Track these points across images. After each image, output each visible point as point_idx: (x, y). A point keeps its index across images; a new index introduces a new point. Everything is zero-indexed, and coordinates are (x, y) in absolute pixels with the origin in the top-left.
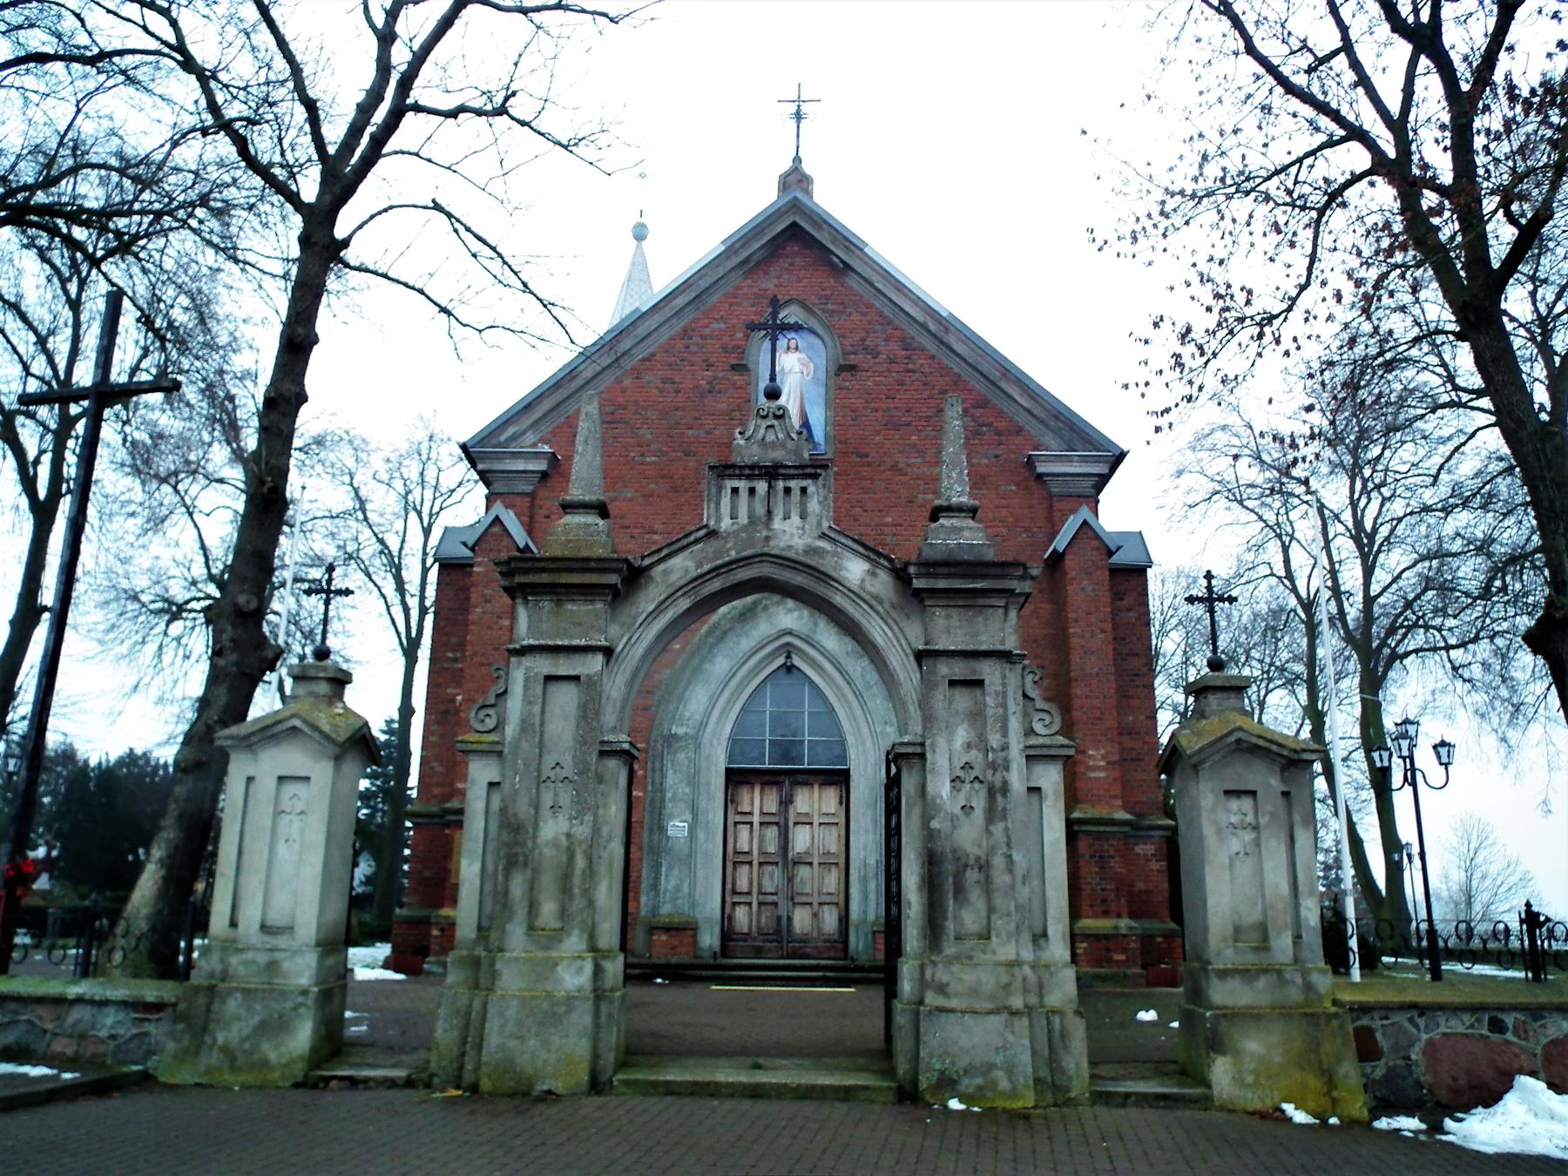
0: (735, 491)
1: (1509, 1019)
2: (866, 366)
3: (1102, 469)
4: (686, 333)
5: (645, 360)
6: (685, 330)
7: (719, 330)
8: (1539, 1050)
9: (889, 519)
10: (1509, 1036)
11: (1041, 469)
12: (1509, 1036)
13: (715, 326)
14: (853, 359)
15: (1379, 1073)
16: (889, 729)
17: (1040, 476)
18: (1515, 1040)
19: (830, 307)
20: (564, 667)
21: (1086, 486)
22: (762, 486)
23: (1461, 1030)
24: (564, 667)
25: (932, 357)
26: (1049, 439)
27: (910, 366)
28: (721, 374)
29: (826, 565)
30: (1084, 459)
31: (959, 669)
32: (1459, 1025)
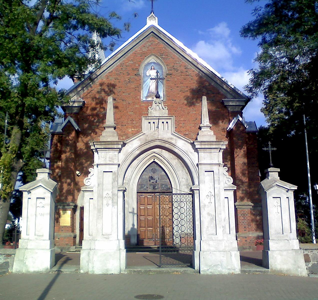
2: (174, 74)
3: (243, 104)
4: (121, 65)
5: (109, 73)
6: (121, 64)
9: (182, 119)
11: (226, 104)
13: (130, 62)
14: (171, 72)
15: (310, 265)
16: (183, 180)
19: (163, 56)
20: (107, 168)
21: (237, 109)
22: (156, 121)
24: (107, 168)
25: (194, 71)
26: (229, 96)
27: (187, 74)
28: (132, 77)
29: (173, 142)
30: (238, 101)
31: (209, 168)
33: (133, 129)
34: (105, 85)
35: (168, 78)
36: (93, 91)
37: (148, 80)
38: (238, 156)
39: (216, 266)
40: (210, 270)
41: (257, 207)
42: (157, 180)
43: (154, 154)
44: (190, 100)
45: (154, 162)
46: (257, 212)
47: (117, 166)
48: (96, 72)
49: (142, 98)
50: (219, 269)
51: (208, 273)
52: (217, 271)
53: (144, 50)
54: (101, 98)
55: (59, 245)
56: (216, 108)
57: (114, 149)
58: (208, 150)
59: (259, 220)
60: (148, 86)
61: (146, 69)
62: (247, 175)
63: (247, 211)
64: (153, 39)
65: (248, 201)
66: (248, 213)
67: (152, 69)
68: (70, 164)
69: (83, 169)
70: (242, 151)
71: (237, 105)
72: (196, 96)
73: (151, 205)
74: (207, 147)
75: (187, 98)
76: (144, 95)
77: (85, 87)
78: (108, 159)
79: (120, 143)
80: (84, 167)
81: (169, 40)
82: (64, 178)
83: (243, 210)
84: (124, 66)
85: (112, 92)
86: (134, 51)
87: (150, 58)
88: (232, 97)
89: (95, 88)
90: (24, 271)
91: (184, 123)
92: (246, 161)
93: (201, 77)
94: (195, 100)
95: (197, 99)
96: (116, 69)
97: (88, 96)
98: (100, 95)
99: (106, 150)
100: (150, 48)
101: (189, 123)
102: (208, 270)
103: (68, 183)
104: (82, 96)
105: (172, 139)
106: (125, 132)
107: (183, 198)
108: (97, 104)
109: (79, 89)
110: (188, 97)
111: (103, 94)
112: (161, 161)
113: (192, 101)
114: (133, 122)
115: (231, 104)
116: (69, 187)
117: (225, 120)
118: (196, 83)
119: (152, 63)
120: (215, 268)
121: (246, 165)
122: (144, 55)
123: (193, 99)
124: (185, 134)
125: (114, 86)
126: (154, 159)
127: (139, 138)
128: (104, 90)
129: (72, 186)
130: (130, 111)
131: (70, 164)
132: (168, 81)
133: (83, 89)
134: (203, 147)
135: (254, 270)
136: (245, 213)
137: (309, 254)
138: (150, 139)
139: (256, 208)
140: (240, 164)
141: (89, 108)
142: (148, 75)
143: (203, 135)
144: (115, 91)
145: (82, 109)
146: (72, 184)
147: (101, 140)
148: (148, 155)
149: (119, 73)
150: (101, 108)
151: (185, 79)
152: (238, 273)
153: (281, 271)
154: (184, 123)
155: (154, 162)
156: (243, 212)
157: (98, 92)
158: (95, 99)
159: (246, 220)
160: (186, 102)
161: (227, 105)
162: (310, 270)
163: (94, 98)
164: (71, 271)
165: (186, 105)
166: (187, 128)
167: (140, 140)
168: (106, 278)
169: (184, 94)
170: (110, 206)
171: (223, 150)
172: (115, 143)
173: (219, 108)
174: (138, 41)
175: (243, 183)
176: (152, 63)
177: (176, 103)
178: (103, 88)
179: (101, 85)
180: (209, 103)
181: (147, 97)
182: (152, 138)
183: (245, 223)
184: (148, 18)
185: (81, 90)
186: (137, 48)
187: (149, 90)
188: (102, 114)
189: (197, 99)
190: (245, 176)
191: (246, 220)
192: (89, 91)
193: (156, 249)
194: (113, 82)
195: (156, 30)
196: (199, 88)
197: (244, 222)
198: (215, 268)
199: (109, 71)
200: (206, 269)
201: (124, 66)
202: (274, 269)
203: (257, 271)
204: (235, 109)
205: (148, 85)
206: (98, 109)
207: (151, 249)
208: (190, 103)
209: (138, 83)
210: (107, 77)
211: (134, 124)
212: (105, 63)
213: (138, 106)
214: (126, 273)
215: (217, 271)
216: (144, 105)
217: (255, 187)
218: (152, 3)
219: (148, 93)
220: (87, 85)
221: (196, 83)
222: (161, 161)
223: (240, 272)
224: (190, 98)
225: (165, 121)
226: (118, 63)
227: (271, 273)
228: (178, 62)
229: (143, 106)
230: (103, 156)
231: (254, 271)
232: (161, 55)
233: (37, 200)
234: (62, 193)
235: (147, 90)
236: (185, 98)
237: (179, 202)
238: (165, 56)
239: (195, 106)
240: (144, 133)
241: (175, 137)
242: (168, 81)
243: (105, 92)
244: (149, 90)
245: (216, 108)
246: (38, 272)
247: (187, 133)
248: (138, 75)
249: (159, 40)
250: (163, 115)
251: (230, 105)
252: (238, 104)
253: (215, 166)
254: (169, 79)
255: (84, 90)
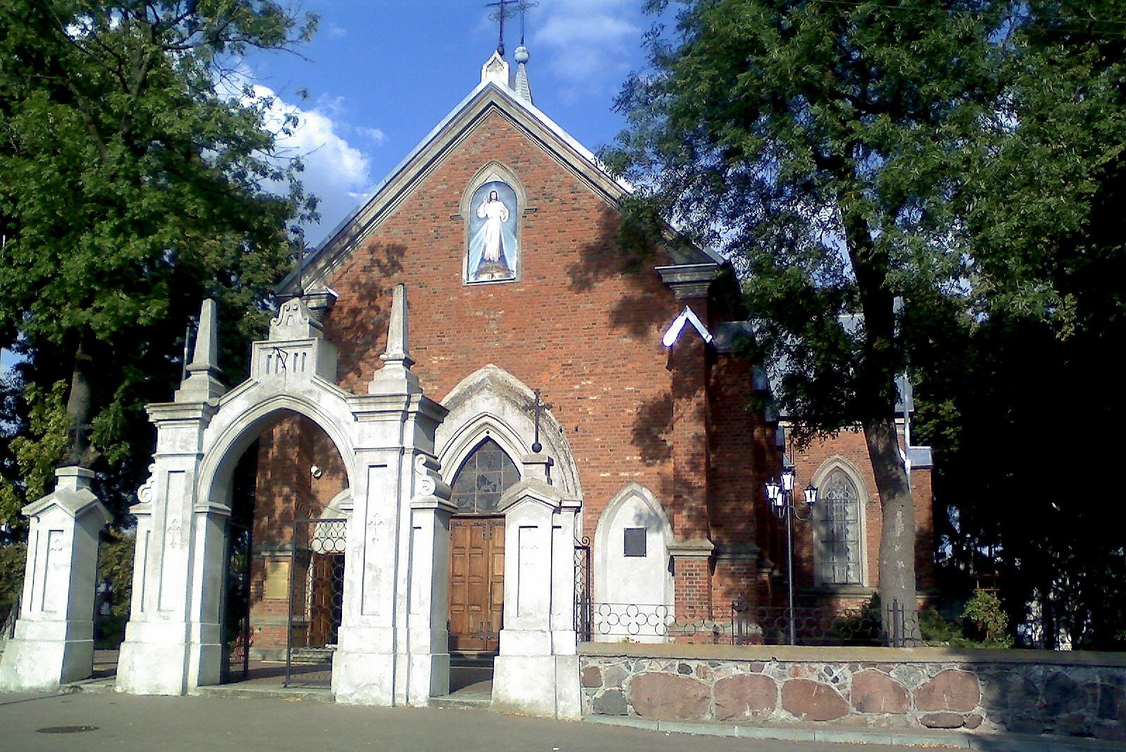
0: (296, 354)
1: (693, 665)
4: (420, 195)
5: (393, 217)
6: (419, 193)
7: (444, 190)
8: (712, 686)
10: (693, 675)
11: (666, 279)
12: (693, 675)
17: (667, 285)
18: (697, 678)
19: (520, 165)
23: (659, 670)
27: (576, 206)
29: (313, 398)
30: (698, 269)
32: (657, 667)
33: (442, 358)
34: (380, 250)
35: (528, 220)
36: (355, 267)
37: (481, 230)
38: (682, 416)
39: (370, 685)
40: (356, 696)
41: (740, 553)
42: (495, 485)
43: (486, 419)
44: (579, 274)
45: (488, 439)
46: (742, 567)
47: (194, 459)
48: (357, 219)
49: (465, 276)
50: (374, 695)
51: (352, 701)
52: (370, 698)
53: (475, 151)
54: (371, 282)
55: (261, 645)
56: (646, 291)
57: (188, 421)
58: (378, 417)
59: (746, 589)
60: (480, 245)
61: (476, 201)
62: (702, 468)
63: (699, 563)
64: (496, 122)
65: (702, 537)
66: (700, 570)
67: (491, 199)
68: (290, 451)
69: (328, 460)
70: (693, 403)
71: (694, 279)
72: (596, 263)
73: (479, 548)
74: (373, 408)
75: (573, 271)
76: (471, 269)
77: (335, 258)
78: (178, 444)
79: (197, 407)
80: (329, 457)
81: (529, 119)
82: (277, 484)
83: (689, 562)
84: (427, 199)
85: (396, 268)
86: (449, 158)
87: (488, 172)
88: (684, 260)
89: (359, 259)
90: (12, 687)
91: (562, 337)
92: (701, 430)
93: (609, 213)
94: (591, 274)
95: (596, 273)
96: (408, 208)
97: (344, 280)
98: (370, 275)
99: (175, 424)
100: (489, 144)
101: (576, 336)
102: (352, 694)
103: (286, 495)
104: (329, 281)
105: (311, 392)
106: (423, 366)
107: (338, 530)
108: (361, 298)
109: (321, 264)
110: (576, 266)
111: (376, 273)
112: (505, 437)
113: (584, 278)
114: (444, 339)
115: (679, 278)
116: (287, 505)
117: (666, 322)
118: (598, 227)
119: (493, 185)
120: (366, 691)
121: (701, 442)
122: (475, 165)
123: (587, 269)
124: (565, 365)
125: (400, 250)
126: (488, 432)
127: (245, 394)
128: (378, 262)
129: (294, 502)
130: (437, 313)
131: (290, 451)
132: (529, 227)
133: (329, 263)
134: (365, 409)
135: (457, 700)
136: (694, 568)
137: (600, 667)
138: (267, 395)
139: (737, 556)
140: (688, 438)
141: (345, 310)
142: (482, 215)
143: (383, 381)
144: (404, 263)
145: (330, 314)
146: (294, 498)
147: (371, 392)
148: (471, 422)
149: (415, 217)
150: (371, 308)
151: (571, 220)
152: (421, 706)
153: (515, 706)
154: (562, 337)
155: (488, 439)
156: (689, 566)
157: (365, 269)
158: (357, 287)
159: (696, 587)
160: (569, 281)
161: (669, 281)
162: (596, 706)
163: (354, 285)
164: (98, 688)
165: (570, 288)
166: (571, 347)
167: (248, 397)
168: (154, 702)
169: (566, 261)
170: (178, 547)
171: (414, 415)
172: (190, 407)
173: (652, 292)
174: (458, 131)
175: (690, 488)
176: (493, 185)
177: (546, 285)
178: (375, 258)
179: (372, 250)
180: (628, 279)
181: (477, 274)
182: (274, 393)
183: (694, 595)
184: (485, 67)
185: (325, 267)
186: (458, 150)
187: (483, 254)
188: (373, 324)
189: (596, 273)
190: (699, 471)
191: (696, 587)
192: (345, 268)
193: (475, 658)
194: (399, 242)
195: (500, 96)
196: (604, 241)
197: (691, 593)
198: (366, 691)
199: (393, 213)
200: (349, 692)
201: (427, 199)
202: (502, 699)
203: (463, 704)
204: (690, 292)
205: (481, 242)
206: (364, 312)
207: (464, 659)
208: (580, 282)
209: (456, 240)
210: (388, 229)
211: (444, 343)
212: (378, 194)
213: (456, 298)
214: (197, 694)
215: (370, 698)
216: (469, 293)
217: (737, 501)
218: (501, 23)
219: (483, 260)
220: (340, 252)
221: (598, 227)
222: (505, 437)
223: (426, 705)
224: (581, 269)
225: (300, 351)
226: (412, 192)
227: (493, 710)
228: (553, 177)
229: (467, 297)
230: (169, 437)
231: (456, 703)
232: (516, 160)
233: (54, 534)
234: (273, 519)
235: (480, 256)
236: (568, 270)
237: (335, 540)
238: (522, 164)
239: (592, 290)
240: (256, 380)
241: (317, 389)
242: (529, 227)
243: (382, 268)
244: (483, 254)
245: (646, 291)
246: (37, 689)
247: (570, 362)
248: (456, 218)
249: (510, 124)
250: (300, 336)
251: (675, 281)
252: (697, 277)
253: (390, 453)
254: (531, 223)
255: (332, 267)
